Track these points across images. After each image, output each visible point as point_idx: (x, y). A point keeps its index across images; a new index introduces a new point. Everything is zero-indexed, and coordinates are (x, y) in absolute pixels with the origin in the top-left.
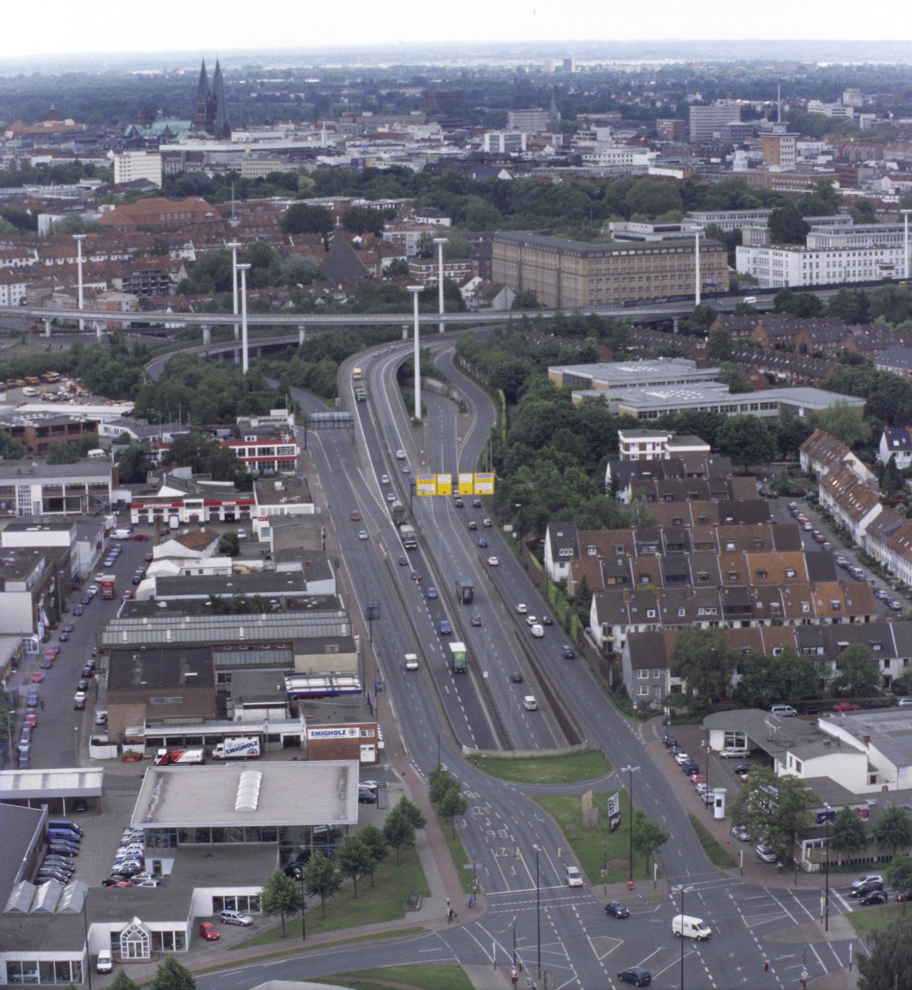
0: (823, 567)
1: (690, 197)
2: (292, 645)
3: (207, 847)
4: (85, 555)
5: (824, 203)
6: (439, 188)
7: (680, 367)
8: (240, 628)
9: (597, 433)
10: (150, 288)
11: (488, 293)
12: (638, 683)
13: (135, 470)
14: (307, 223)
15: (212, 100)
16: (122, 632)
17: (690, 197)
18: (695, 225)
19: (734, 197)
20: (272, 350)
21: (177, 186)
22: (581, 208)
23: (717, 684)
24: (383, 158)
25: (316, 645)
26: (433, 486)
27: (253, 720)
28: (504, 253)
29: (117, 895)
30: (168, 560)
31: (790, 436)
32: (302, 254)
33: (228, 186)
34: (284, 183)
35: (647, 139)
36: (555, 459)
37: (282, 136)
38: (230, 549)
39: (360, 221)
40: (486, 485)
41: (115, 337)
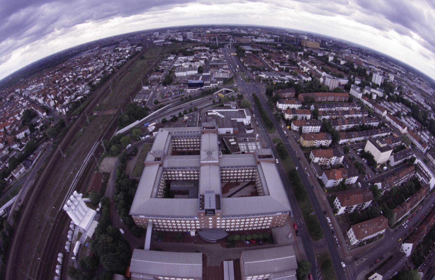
0: (261, 61)
1: (249, 35)
2: (223, 65)
3: (219, 79)
4: (207, 58)
5: (258, 36)
6: (231, 33)
7: (249, 47)
8: (220, 64)
9: (244, 51)
10: (210, 40)
11: (234, 41)
12: (248, 69)
13: (210, 52)
14: (222, 36)
15: (213, 27)
16: (211, 64)
17: (249, 35)
18: (250, 37)
19: (252, 35)
20: (219, 44)
21: (211, 33)
22: (241, 35)
23: (254, 69)
24: (226, 31)
25: (225, 65)
26: (232, 54)
27: (221, 70)
28: (236, 38)
29: (212, 82)
30: (213, 59)
31: (257, 52)
32: (221, 38)
33: (215, 33)
34: (219, 33)
35: (245, 31)
36: (240, 53)
37: (218, 30)
38: (218, 58)
39: (225, 36)
40: (236, 54)
41: (208, 43)
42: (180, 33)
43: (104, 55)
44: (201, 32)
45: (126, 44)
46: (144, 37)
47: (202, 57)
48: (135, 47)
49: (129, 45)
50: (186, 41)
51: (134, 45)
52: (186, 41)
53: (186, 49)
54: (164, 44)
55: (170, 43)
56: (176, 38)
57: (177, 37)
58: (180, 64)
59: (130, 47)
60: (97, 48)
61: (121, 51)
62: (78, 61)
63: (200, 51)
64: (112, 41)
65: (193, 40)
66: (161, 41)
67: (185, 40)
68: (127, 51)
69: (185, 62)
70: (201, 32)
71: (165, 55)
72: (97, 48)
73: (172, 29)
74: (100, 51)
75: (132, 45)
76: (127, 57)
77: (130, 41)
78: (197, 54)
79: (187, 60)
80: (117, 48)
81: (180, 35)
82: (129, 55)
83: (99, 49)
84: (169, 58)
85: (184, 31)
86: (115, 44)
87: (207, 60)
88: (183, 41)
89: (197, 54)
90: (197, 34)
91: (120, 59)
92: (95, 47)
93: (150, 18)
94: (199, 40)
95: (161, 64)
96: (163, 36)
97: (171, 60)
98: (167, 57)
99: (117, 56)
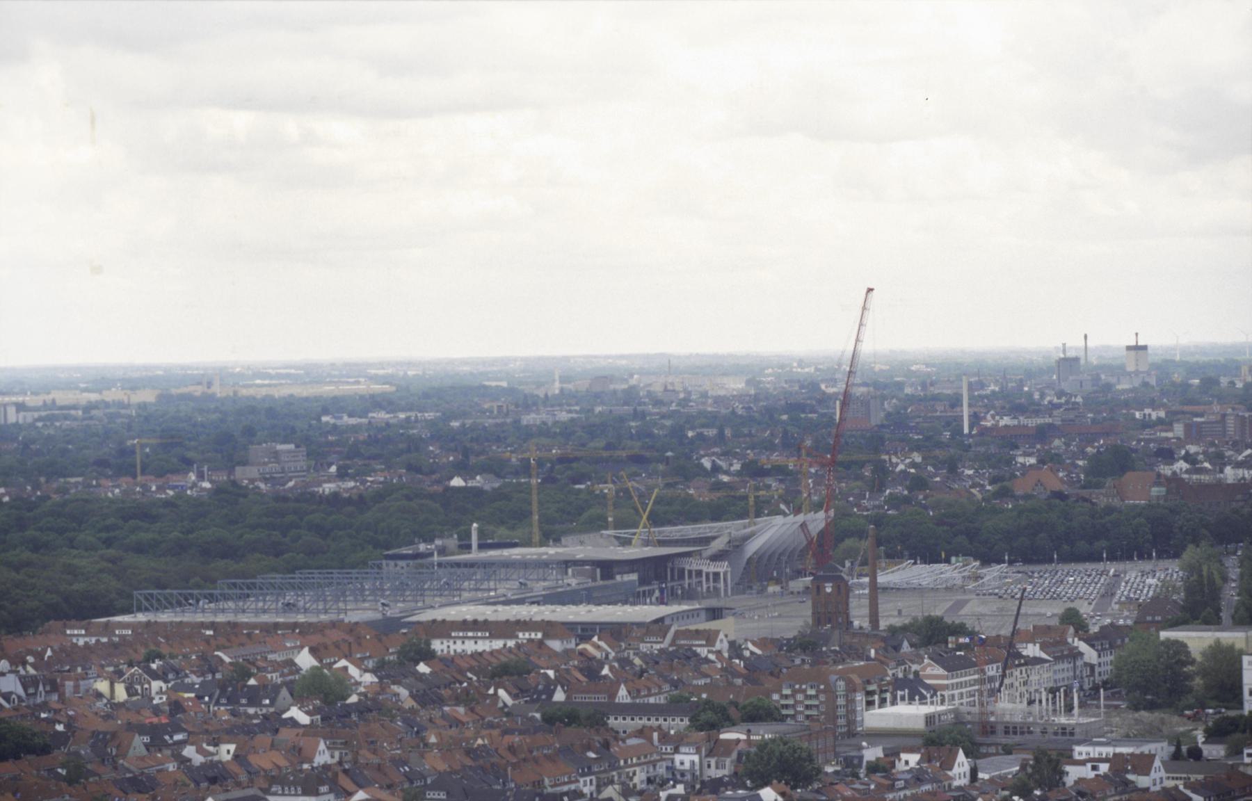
43: (907, 714)
60: (773, 531)
62: (323, 692)
72: (773, 531)
74: (831, 612)
83: (822, 555)
92: (727, 506)
93: (465, 625)
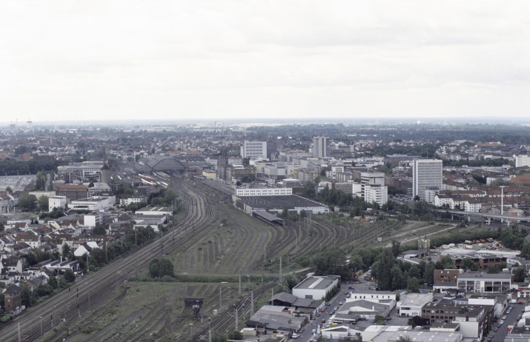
41: (514, 226)
42: (380, 161)
44: (489, 163)
45: (92, 180)
46: (190, 158)
47: (472, 302)
48: (134, 208)
49: (105, 186)
50: (404, 206)
51: (130, 194)
52: (405, 209)
53: (397, 251)
54: (284, 215)
55: (321, 209)
56: (356, 189)
57: (358, 181)
58: (353, 332)
59: (108, 202)
61: (58, 214)
63: (471, 265)
64: (22, 150)
65: (438, 202)
66: (273, 192)
67: (399, 200)
68: (90, 221)
69: (379, 320)
70: (489, 163)
71: (282, 274)
73: (339, 138)
75: (119, 191)
76: (80, 251)
77: (111, 166)
78: (451, 280)
79: (395, 310)
80: (38, 195)
81: (380, 169)
82: (93, 245)
84: (299, 292)
85: (400, 150)
86: (31, 169)
87: (496, 319)
88: (390, 207)
89: (451, 280)
90: (469, 170)
91: (46, 258)
94: (469, 207)
95: (255, 318)
96: (291, 168)
97: (311, 305)
98: (291, 285)
99: (30, 236)
